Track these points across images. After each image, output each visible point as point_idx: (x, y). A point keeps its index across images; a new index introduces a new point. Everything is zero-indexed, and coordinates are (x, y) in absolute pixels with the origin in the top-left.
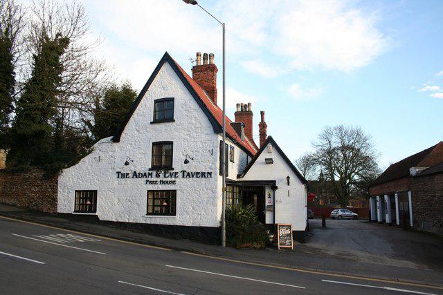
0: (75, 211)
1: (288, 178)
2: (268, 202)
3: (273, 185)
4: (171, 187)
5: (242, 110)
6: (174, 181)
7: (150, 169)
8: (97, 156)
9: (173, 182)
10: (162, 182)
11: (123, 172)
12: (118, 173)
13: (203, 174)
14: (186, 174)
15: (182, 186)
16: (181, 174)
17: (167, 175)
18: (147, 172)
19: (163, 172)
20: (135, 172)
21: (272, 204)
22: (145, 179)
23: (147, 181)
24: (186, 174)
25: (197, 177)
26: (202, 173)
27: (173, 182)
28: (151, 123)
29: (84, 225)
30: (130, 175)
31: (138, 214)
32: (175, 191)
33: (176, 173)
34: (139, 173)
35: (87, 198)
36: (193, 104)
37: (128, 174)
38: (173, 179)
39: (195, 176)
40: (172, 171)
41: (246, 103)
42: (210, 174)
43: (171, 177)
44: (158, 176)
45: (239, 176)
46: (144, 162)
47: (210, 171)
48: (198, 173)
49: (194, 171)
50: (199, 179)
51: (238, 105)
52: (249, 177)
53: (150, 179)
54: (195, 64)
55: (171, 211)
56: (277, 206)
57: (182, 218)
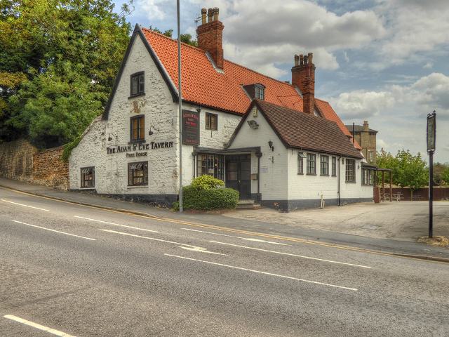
0: (82, 187)
1: (270, 143)
2: (254, 170)
3: (258, 152)
4: (142, 159)
5: (301, 63)
9: (145, 154)
10: (138, 155)
11: (156, 142)
12: (108, 148)
13: (166, 144)
14: (154, 145)
15: (153, 156)
16: (150, 146)
18: (127, 146)
21: (257, 172)
22: (125, 153)
23: (127, 154)
24: (154, 145)
28: (129, 98)
30: (116, 150)
31: (123, 186)
32: (147, 162)
33: (147, 145)
35: (89, 174)
36: (158, 76)
37: (114, 149)
38: (145, 151)
42: (171, 143)
44: (134, 149)
46: (125, 139)
47: (171, 140)
48: (163, 144)
49: (159, 141)
50: (163, 149)
51: (296, 58)
52: (237, 144)
53: (129, 153)
54: (200, 23)
55: (144, 183)
56: (262, 176)
57: (152, 188)
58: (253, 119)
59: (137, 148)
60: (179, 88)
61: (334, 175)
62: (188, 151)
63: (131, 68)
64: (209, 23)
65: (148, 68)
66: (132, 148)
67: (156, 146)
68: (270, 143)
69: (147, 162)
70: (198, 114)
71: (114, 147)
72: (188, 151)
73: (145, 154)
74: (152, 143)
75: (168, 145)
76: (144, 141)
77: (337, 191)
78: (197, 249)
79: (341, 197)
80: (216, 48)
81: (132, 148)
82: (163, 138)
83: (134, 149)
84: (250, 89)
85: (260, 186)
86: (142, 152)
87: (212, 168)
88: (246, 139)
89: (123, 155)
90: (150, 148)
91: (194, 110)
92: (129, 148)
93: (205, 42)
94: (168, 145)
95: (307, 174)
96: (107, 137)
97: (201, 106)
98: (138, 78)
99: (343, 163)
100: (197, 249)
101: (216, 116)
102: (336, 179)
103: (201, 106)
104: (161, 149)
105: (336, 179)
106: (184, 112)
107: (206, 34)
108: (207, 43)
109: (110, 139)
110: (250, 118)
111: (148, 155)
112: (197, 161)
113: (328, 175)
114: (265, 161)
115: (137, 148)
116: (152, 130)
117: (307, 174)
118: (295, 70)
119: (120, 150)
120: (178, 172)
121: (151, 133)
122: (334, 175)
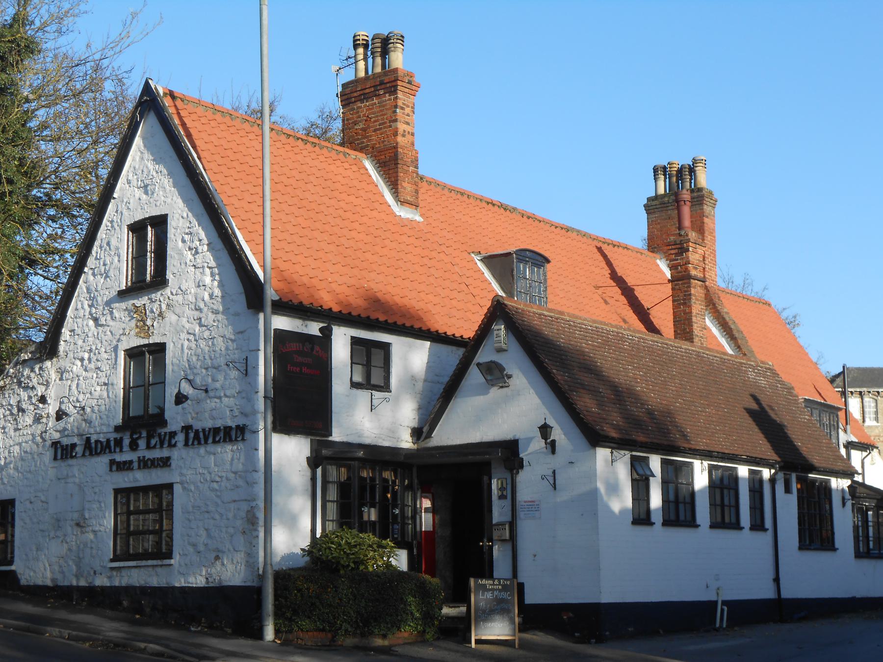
1: (545, 430)
2: (499, 512)
3: (509, 453)
4: (156, 477)
6: (168, 458)
7: (117, 429)
8: (13, 401)
10: (145, 464)
11: (198, 425)
13: (228, 430)
14: (192, 435)
16: (180, 438)
17: (153, 442)
18: (113, 436)
19: (144, 434)
20: (88, 439)
21: (508, 518)
22: (104, 460)
23: (112, 462)
24: (192, 435)
25: (214, 442)
26: (226, 428)
27: (165, 462)
29: (236, 286)
30: (79, 449)
32: (170, 487)
33: (173, 434)
34: (97, 442)
37: (74, 446)
38: (165, 453)
39: (210, 440)
40: (163, 431)
41: (682, 159)
42: (241, 430)
43: (162, 446)
44: (134, 446)
45: (417, 433)
47: (241, 421)
53: (119, 458)
56: (527, 528)
57: (188, 572)
58: (495, 357)
59: (142, 443)
60: (263, 267)
61: (758, 526)
62: (290, 452)
63: (130, 201)
64: (367, 78)
65: (172, 202)
66: (126, 442)
67: (198, 437)
68: (545, 430)
69: (170, 487)
70: (327, 334)
71: (76, 440)
72: (290, 452)
73: (165, 462)
74: (187, 429)
75: (235, 434)
76: (164, 423)
77: (771, 575)
78: (153, 647)
79: (786, 594)
80: (396, 148)
81: (126, 442)
82: (221, 411)
83: (134, 446)
84: (502, 264)
85: (520, 557)
86: (157, 454)
87: (373, 505)
88: (472, 422)
89: (102, 462)
90: (180, 444)
91: (314, 328)
92: (119, 443)
93: (364, 130)
94: (235, 434)
95: (713, 526)
96: (52, 408)
97: (332, 317)
98: (151, 231)
99: (788, 490)
100: (153, 647)
101: (385, 348)
102: (766, 538)
103: (332, 317)
104: (211, 448)
105: (766, 538)
106: (281, 336)
107: (363, 106)
108: (370, 132)
109: (60, 415)
110: (484, 355)
111: (174, 463)
112: (325, 483)
113: (736, 526)
114: (529, 482)
115: (142, 443)
116: (186, 389)
117: (713, 526)
118: (655, 207)
119: (92, 448)
120: (261, 516)
121: (180, 399)
122: (758, 526)
